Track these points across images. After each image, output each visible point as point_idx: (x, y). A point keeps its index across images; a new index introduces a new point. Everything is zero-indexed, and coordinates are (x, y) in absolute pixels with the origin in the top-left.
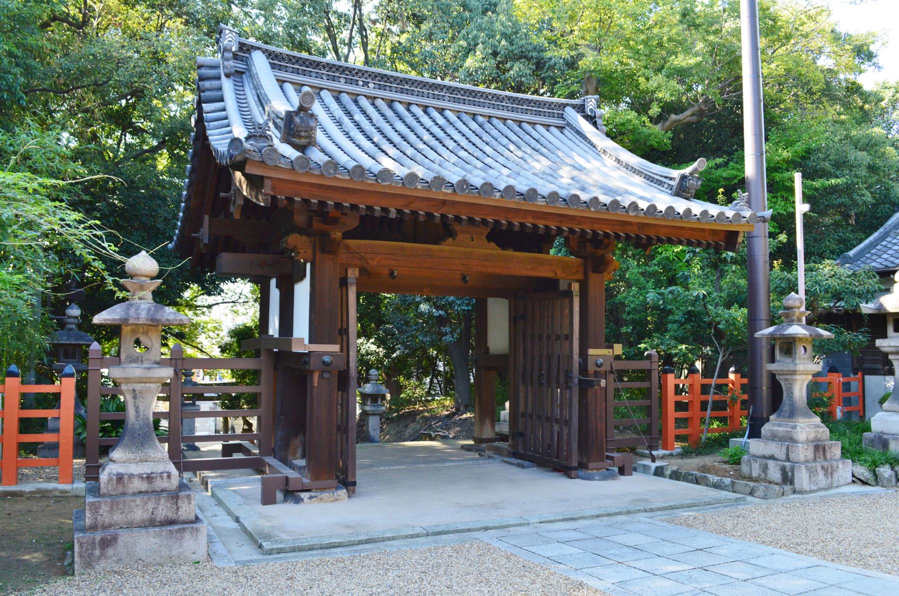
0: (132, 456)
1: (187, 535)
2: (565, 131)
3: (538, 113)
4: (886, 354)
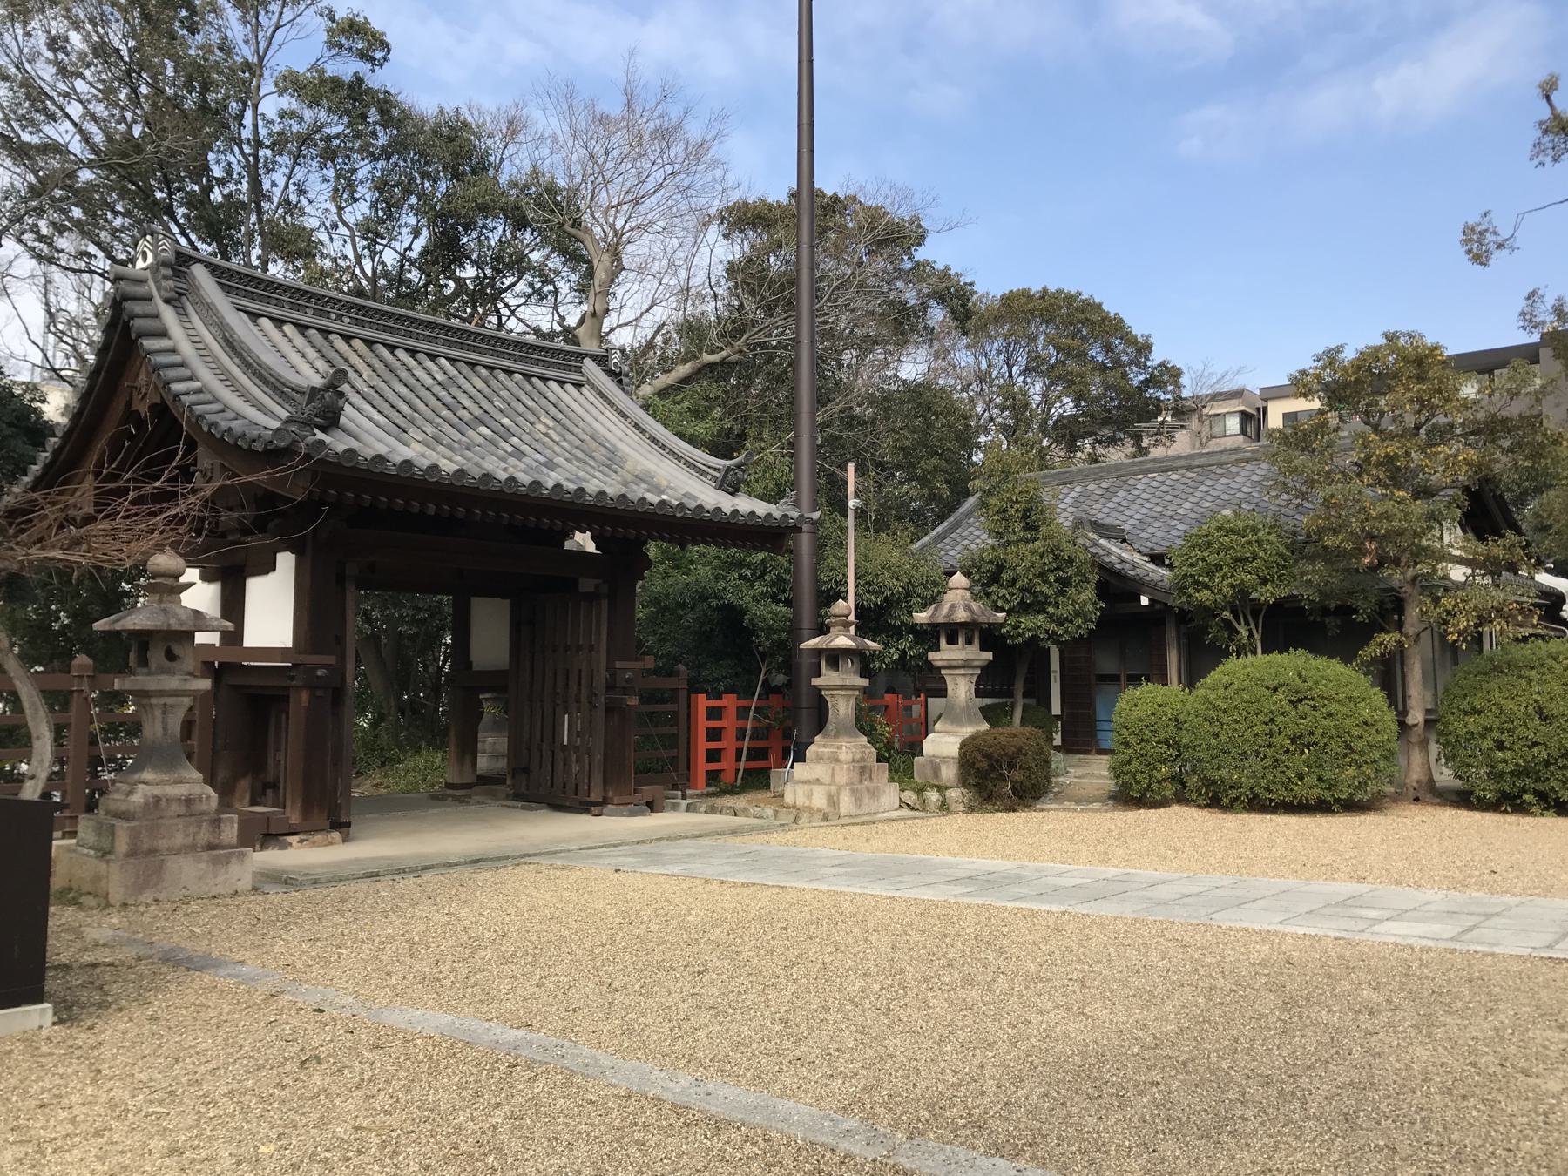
0: (166, 778)
1: (234, 860)
2: (584, 390)
3: (551, 365)
4: (939, 668)
